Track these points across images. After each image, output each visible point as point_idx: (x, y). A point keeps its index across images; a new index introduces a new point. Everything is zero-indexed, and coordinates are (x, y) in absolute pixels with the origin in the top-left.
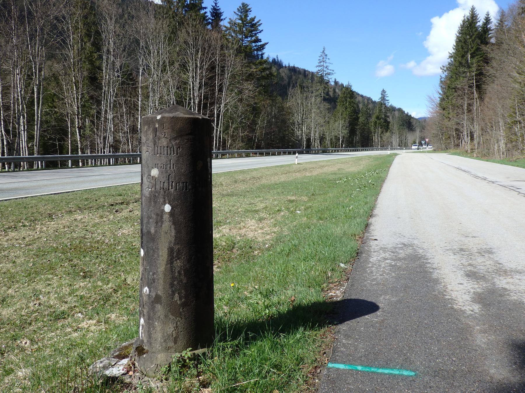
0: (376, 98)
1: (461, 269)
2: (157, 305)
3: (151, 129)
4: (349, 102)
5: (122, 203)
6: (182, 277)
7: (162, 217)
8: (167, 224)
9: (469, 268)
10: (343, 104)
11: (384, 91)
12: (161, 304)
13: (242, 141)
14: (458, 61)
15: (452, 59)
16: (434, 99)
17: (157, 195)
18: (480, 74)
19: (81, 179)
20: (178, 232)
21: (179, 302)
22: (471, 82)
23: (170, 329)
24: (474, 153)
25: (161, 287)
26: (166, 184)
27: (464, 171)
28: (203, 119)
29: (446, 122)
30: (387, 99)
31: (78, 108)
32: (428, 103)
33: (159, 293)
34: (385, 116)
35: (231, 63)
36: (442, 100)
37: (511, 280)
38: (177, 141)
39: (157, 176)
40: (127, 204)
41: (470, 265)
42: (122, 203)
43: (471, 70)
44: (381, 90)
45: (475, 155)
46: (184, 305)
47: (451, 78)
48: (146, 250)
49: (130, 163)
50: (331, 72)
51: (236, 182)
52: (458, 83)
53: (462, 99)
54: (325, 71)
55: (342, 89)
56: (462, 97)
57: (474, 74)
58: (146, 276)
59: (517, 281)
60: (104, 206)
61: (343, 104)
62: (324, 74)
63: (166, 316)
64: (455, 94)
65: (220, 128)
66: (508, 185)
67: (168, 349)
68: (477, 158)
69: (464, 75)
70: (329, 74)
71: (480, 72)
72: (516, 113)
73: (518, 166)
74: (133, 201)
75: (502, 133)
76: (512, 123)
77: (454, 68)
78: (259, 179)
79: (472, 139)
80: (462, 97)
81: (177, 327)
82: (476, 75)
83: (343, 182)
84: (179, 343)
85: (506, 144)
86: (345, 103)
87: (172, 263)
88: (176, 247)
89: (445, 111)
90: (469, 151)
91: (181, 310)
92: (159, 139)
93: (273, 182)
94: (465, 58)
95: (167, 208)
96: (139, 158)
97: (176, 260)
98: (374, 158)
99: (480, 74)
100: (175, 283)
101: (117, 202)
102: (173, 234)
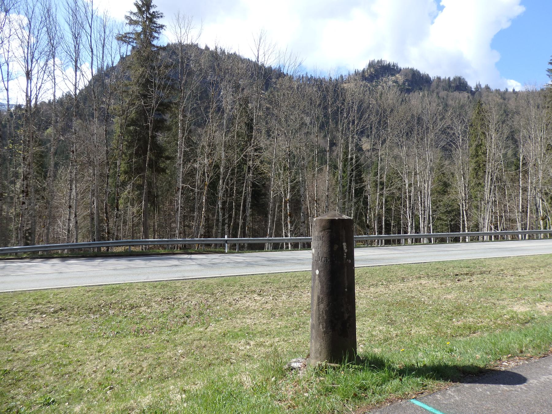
19: (441, 253)
20: (322, 287)
26: (317, 258)
28: (339, 219)
31: (465, 194)
38: (322, 233)
60: (449, 275)
63: (316, 337)
87: (319, 305)
88: (321, 296)
101: (462, 273)
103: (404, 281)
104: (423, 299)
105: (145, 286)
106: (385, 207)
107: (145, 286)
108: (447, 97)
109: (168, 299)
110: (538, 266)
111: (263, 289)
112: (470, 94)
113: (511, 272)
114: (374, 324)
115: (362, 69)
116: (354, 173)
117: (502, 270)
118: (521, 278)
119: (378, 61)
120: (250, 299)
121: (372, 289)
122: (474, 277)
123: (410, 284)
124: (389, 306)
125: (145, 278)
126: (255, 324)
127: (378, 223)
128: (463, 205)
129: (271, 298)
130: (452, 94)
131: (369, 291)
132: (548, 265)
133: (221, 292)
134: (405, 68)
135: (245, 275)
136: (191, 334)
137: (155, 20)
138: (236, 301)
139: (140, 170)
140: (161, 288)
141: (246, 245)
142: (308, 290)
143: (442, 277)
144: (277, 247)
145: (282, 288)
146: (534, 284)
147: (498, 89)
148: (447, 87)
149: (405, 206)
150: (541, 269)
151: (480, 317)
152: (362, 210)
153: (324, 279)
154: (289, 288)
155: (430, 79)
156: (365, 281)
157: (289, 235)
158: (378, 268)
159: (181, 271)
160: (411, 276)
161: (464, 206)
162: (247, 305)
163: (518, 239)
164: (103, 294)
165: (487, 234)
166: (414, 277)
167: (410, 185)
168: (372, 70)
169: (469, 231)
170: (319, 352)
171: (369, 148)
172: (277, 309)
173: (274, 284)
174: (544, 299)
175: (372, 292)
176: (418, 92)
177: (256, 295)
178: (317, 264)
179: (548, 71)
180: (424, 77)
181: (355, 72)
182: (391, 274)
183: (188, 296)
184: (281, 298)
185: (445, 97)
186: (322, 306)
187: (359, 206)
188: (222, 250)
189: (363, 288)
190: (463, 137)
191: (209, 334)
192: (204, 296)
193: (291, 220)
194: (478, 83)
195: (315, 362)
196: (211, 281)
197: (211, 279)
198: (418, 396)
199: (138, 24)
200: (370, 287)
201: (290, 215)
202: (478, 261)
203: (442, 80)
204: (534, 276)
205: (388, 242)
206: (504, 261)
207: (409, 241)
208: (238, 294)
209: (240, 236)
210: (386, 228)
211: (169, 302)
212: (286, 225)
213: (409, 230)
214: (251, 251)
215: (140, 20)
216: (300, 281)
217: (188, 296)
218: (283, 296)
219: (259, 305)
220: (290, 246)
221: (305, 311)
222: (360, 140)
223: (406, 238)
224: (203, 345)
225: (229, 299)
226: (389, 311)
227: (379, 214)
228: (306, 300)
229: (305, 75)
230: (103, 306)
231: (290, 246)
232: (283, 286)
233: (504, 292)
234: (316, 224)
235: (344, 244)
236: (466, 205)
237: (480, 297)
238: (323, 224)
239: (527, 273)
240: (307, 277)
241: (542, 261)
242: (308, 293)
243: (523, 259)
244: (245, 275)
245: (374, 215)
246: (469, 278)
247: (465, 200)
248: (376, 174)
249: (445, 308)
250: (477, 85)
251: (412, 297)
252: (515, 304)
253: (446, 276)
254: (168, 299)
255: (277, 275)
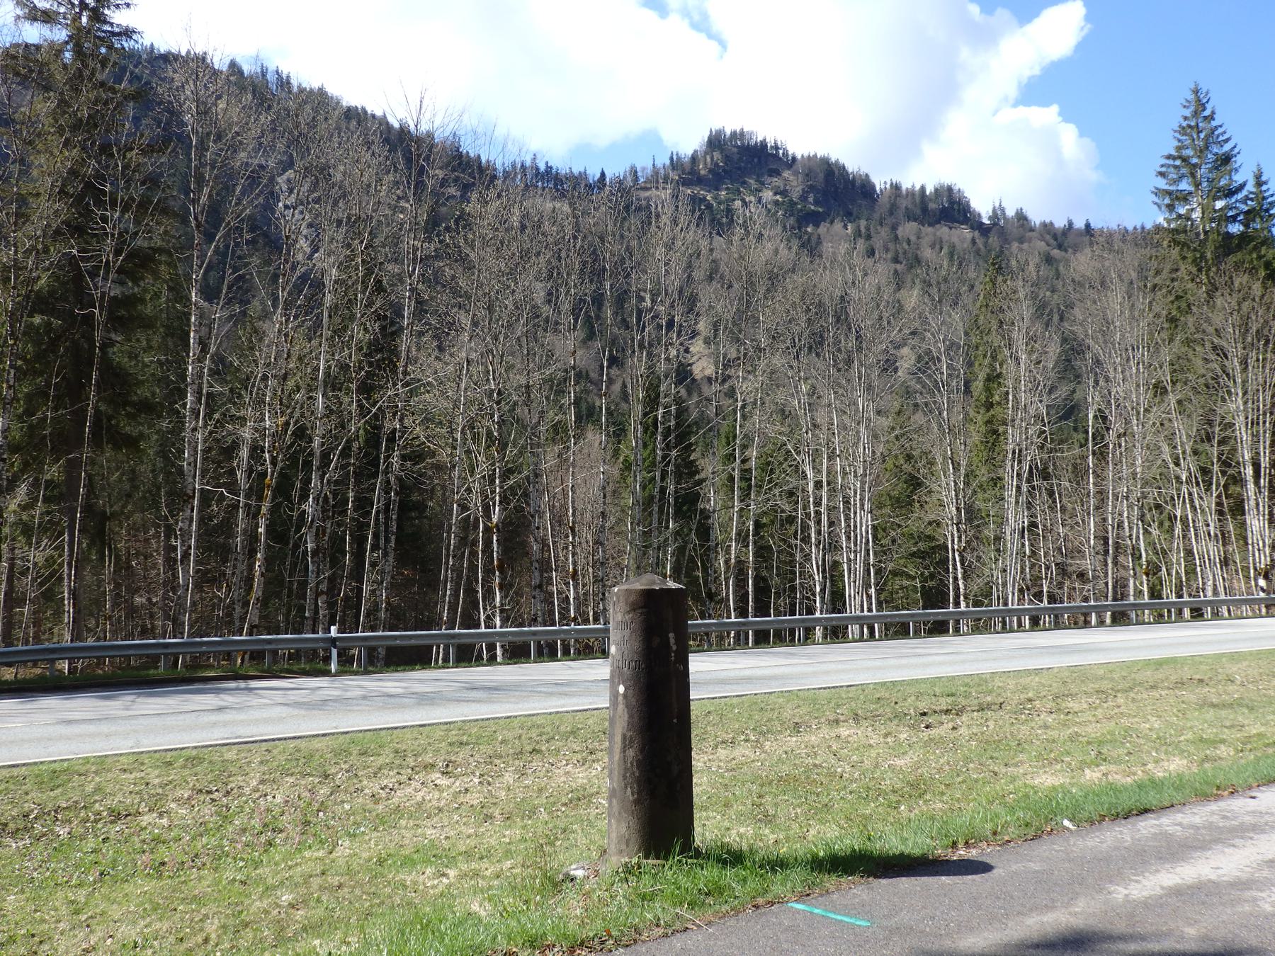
5: (947, 712)
19: (904, 661)
20: (631, 717)
28: (661, 590)
31: (958, 509)
42: (947, 712)
49: (1075, 625)
60: (906, 715)
63: (619, 813)
67: (621, 852)
74: (974, 708)
87: (625, 752)
88: (629, 734)
101: (938, 709)
103: (799, 732)
104: (839, 770)
105: (142, 764)
106: (755, 543)
107: (142, 764)
108: (918, 238)
109: (209, 792)
110: (1112, 689)
111: (453, 759)
112: (977, 233)
113: (1050, 705)
114: (726, 824)
115: (690, 152)
116: (674, 453)
117: (1030, 700)
118: (1070, 717)
119: (734, 134)
120: (423, 783)
121: (722, 753)
122: (964, 718)
123: (813, 738)
124: (762, 785)
125: (131, 743)
126: (447, 838)
127: (737, 586)
128: (952, 536)
129: (476, 780)
130: (930, 229)
131: (714, 757)
132: (1135, 685)
133: (348, 771)
134: (806, 155)
135: (404, 727)
136: (297, 864)
137: (106, 12)
138: (387, 790)
139: (65, 441)
140: (184, 767)
141: (382, 652)
142: (567, 758)
143: (890, 720)
144: (466, 655)
145: (500, 757)
146: (1093, 731)
147: (1048, 221)
148: (918, 212)
149: (806, 539)
150: (1119, 695)
151: (958, 800)
152: (695, 551)
153: (633, 701)
154: (519, 754)
155: (873, 187)
156: (706, 733)
157: (498, 621)
158: (735, 701)
159: (225, 724)
160: (816, 718)
161: (956, 540)
162: (419, 798)
163: (1087, 624)
164: (28, 787)
165: (856, 619)
166: (823, 720)
167: (818, 485)
168: (717, 155)
169: (968, 606)
170: (624, 840)
171: (710, 371)
172: (495, 804)
173: (481, 747)
174: (1105, 760)
175: (723, 758)
176: (842, 221)
177: (438, 775)
178: (621, 674)
179: (1156, 194)
180: (858, 183)
181: (671, 158)
182: (769, 715)
183: (262, 782)
184: (501, 779)
185: (913, 238)
186: (631, 753)
187: (686, 543)
188: (321, 665)
189: (701, 750)
190: (951, 360)
191: (341, 862)
192: (303, 783)
193: (503, 578)
194: (997, 205)
195: (616, 860)
196: (316, 744)
197: (317, 740)
198: (803, 897)
199: (56, 22)
200: (716, 747)
201: (501, 568)
202: (976, 679)
203: (904, 192)
204: (1099, 712)
205: (762, 639)
206: (1037, 679)
207: (819, 632)
208: (391, 773)
209: (364, 627)
210: (756, 600)
211: (213, 800)
212: (489, 594)
213: (818, 605)
214: (402, 668)
215: (62, 10)
216: (544, 737)
217: (262, 782)
218: (507, 774)
219: (450, 797)
220: (499, 652)
221: (565, 805)
222: (687, 351)
223: (808, 625)
224: (336, 883)
225: (371, 787)
226: (760, 796)
227: (739, 562)
228: (564, 782)
229: (528, 163)
230: (36, 818)
231: (499, 652)
232: (502, 750)
233: (1024, 749)
234: (618, 598)
235: (671, 635)
236: (960, 537)
237: (967, 760)
238: (632, 598)
239: (1085, 706)
240: (562, 728)
241: (1124, 678)
242: (567, 765)
243: (1080, 674)
244: (404, 727)
245: (727, 562)
246: (952, 720)
247: (957, 524)
248: (730, 458)
249: (886, 785)
250: (994, 210)
251: (815, 766)
252: (1041, 771)
253: (899, 717)
254: (209, 792)
255: (484, 724)
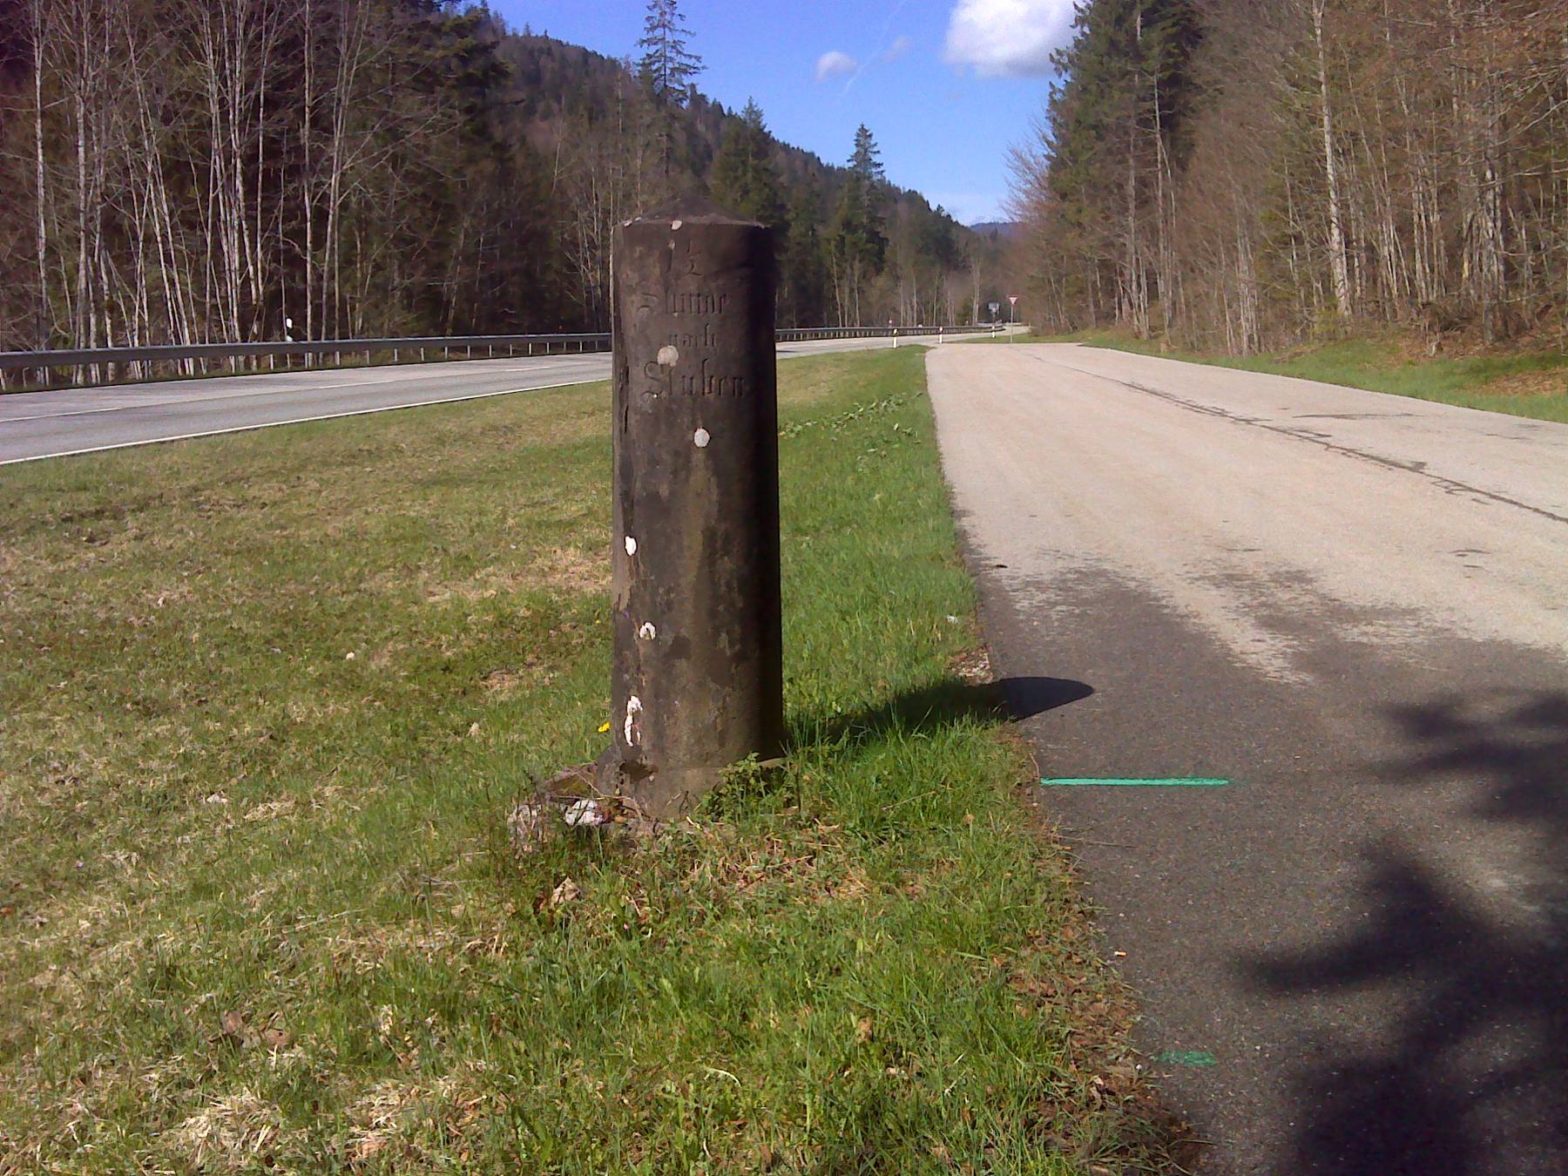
0: (837, 154)
1: (1247, 614)
2: (678, 663)
3: (657, 253)
4: (755, 169)
5: (99, 514)
6: (735, 595)
7: (688, 460)
8: (700, 477)
9: (1264, 612)
10: (736, 178)
11: (864, 134)
12: (688, 658)
13: (409, 308)
14: (1106, 34)
15: (1086, 30)
16: (1032, 161)
17: (674, 407)
18: (1175, 81)
21: (728, 653)
22: (1147, 105)
23: (710, 713)
24: (1161, 339)
25: (687, 621)
27: (1154, 393)
29: (1071, 239)
30: (876, 159)
32: (1013, 177)
33: (684, 632)
34: (873, 220)
35: (360, 29)
36: (1057, 165)
37: (1370, 629)
38: (720, 282)
39: (673, 364)
40: (115, 518)
41: (1263, 605)
42: (99, 514)
43: (1145, 67)
44: (855, 129)
45: (1163, 347)
46: (739, 658)
47: (1079, 91)
48: (644, 537)
50: (692, 62)
51: (441, 441)
52: (1106, 108)
53: (1120, 162)
54: (672, 59)
55: (716, 125)
56: (1119, 157)
57: (1154, 80)
58: (648, 599)
59: (1383, 630)
61: (736, 178)
62: (668, 71)
63: (701, 685)
64: (1100, 146)
65: (330, 258)
66: (1292, 429)
68: (1171, 354)
69: (1123, 83)
70: (685, 72)
71: (1174, 75)
72: (1286, 211)
73: (1301, 376)
75: (1244, 272)
76: (1275, 240)
77: (1094, 57)
78: (512, 431)
79: (1153, 294)
80: (1119, 157)
81: (724, 708)
82: (1161, 83)
83: (793, 435)
84: (729, 746)
85: (1258, 309)
86: (740, 172)
87: (712, 563)
88: (723, 527)
89: (1066, 205)
90: (1145, 336)
91: (733, 670)
92: (678, 277)
93: (559, 439)
94: (1126, 25)
95: (701, 438)
96: (191, 360)
97: (722, 556)
98: (852, 361)
99: (1175, 81)
100: (721, 608)
102: (715, 497)
